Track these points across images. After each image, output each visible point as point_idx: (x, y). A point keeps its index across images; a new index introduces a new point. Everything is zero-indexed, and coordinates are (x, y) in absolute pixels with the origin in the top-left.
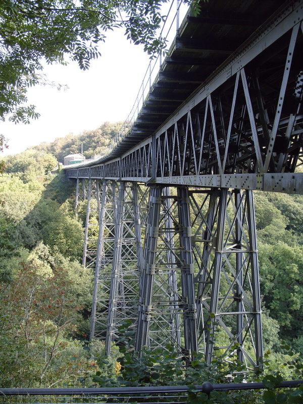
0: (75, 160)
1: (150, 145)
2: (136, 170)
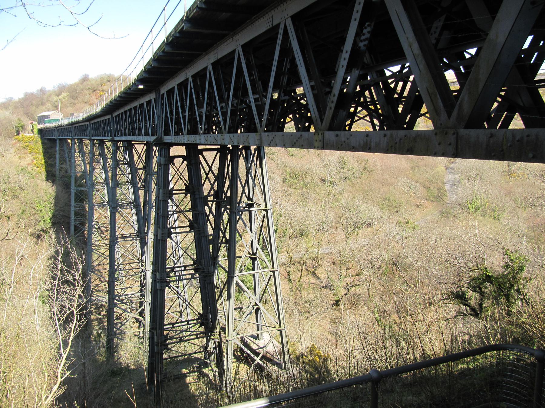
0: (51, 118)
1: (153, 101)
2: (102, 132)
